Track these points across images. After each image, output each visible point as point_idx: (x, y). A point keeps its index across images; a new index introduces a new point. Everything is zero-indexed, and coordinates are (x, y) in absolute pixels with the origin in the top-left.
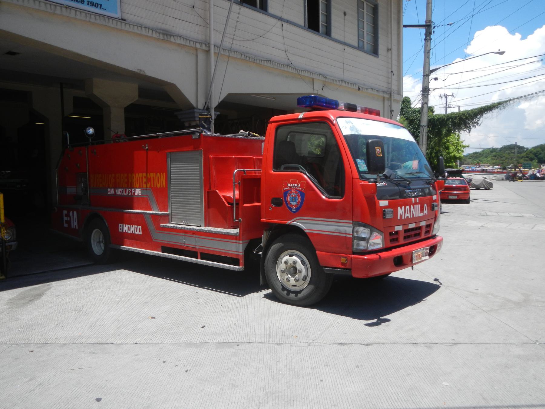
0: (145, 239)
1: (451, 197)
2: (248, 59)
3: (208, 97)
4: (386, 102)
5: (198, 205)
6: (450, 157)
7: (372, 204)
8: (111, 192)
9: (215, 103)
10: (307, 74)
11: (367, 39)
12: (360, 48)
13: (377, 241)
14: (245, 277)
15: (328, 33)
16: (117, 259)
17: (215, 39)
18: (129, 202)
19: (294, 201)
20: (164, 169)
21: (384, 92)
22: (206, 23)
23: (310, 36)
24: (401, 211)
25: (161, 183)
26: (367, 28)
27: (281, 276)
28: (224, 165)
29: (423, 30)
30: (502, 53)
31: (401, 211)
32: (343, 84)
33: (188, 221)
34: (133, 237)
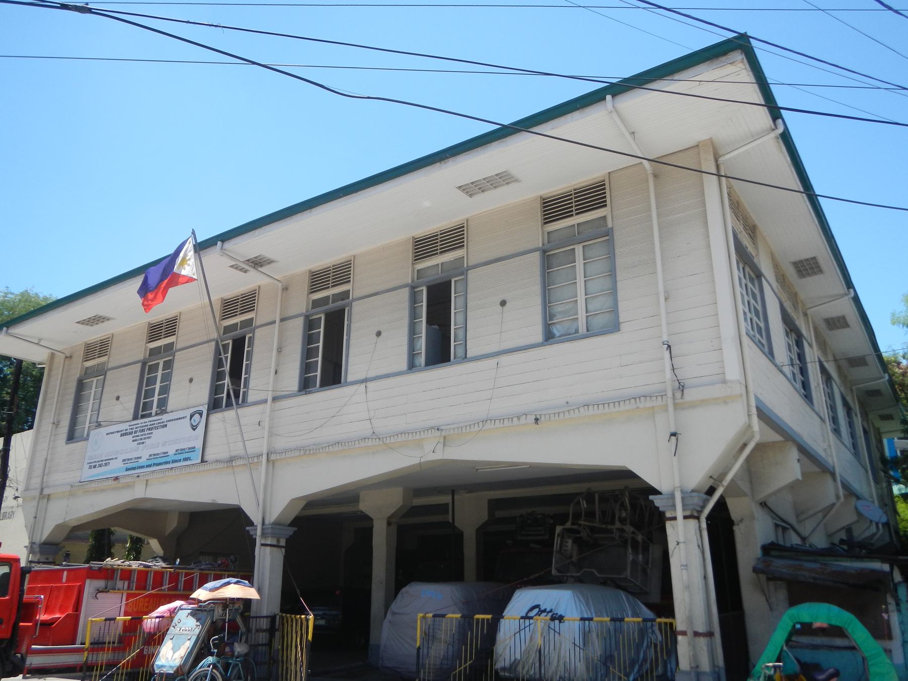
10: (400, 439)
32: (488, 426)
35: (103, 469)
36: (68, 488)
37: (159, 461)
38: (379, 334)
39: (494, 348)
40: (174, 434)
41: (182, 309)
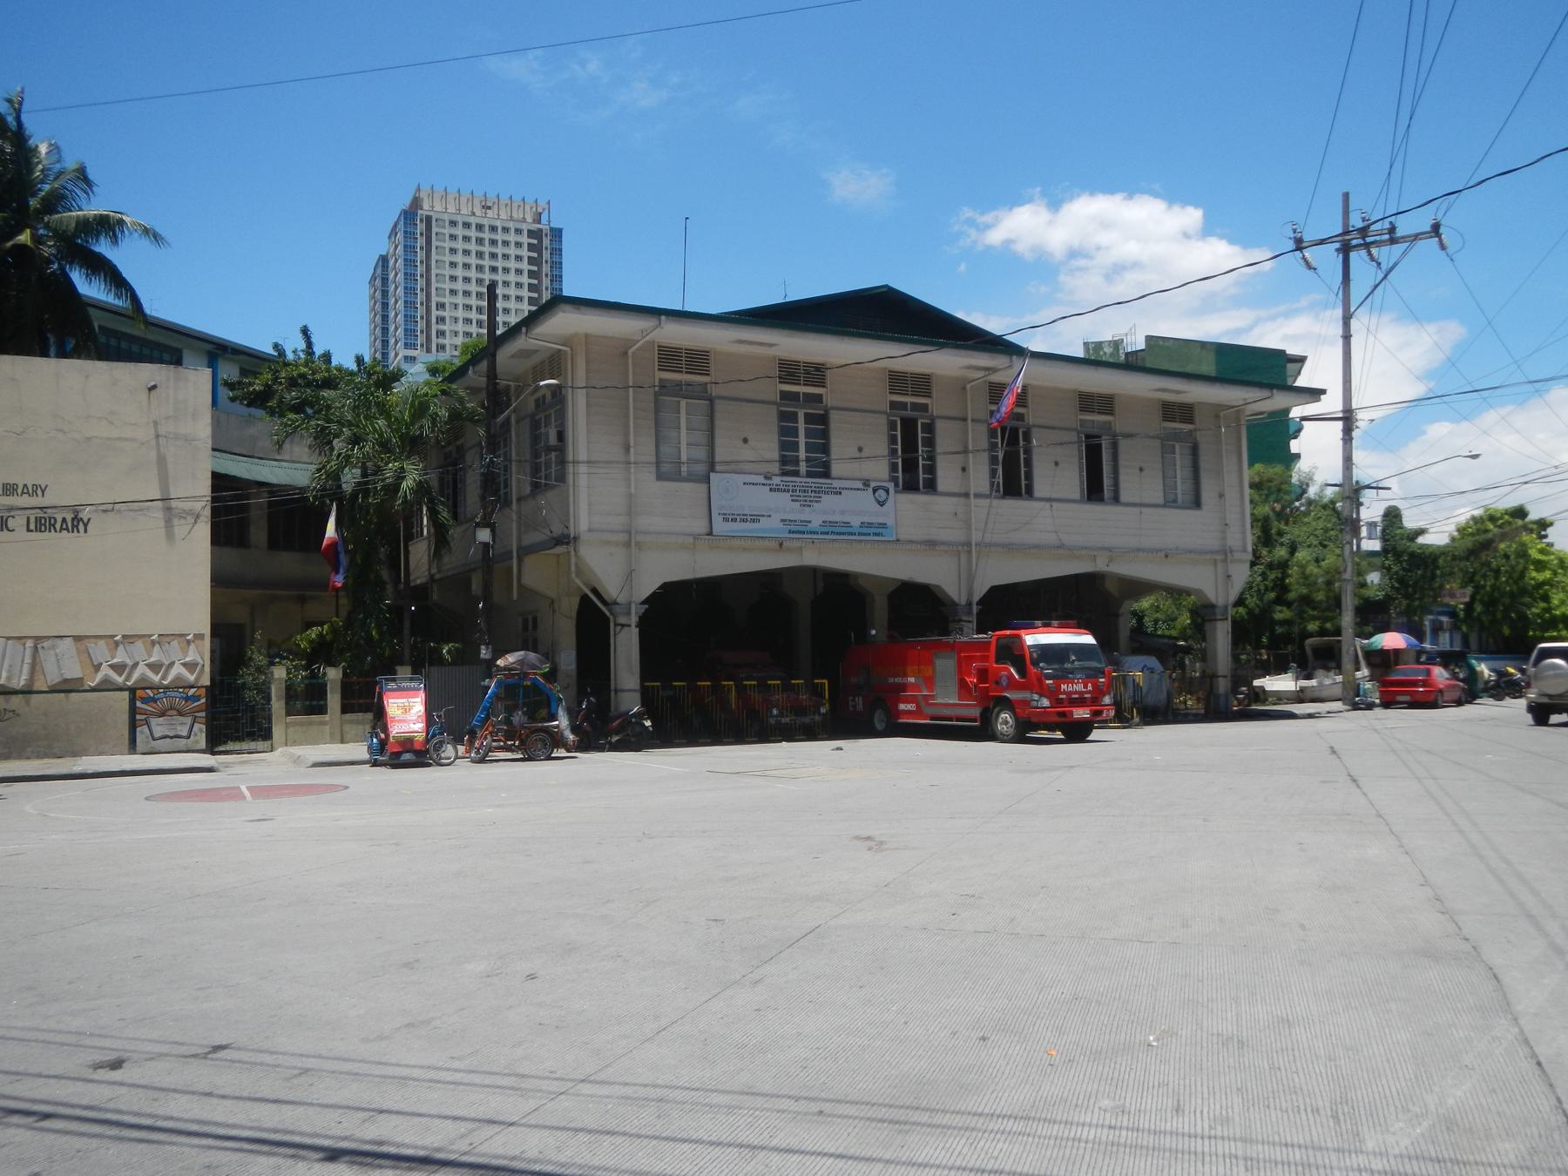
0: (918, 713)
1: (1400, 698)
2: (1010, 548)
3: (970, 593)
4: (1220, 565)
5: (953, 687)
6: (553, 705)
7: (1041, 682)
8: (891, 680)
9: (976, 598)
11: (1182, 488)
12: (1170, 502)
13: (1046, 702)
14: (982, 731)
15: (1116, 499)
16: (897, 729)
17: (976, 537)
18: (904, 687)
19: (1004, 682)
20: (930, 663)
21: (1212, 552)
22: (968, 524)
24: (1064, 687)
26: (1182, 473)
29: (1340, 424)
30: (1475, 457)
31: (1064, 687)
33: (947, 698)
34: (909, 712)
36: (691, 539)
37: (836, 531)
38: (1057, 464)
39: (1138, 501)
40: (850, 505)
41: (938, 372)
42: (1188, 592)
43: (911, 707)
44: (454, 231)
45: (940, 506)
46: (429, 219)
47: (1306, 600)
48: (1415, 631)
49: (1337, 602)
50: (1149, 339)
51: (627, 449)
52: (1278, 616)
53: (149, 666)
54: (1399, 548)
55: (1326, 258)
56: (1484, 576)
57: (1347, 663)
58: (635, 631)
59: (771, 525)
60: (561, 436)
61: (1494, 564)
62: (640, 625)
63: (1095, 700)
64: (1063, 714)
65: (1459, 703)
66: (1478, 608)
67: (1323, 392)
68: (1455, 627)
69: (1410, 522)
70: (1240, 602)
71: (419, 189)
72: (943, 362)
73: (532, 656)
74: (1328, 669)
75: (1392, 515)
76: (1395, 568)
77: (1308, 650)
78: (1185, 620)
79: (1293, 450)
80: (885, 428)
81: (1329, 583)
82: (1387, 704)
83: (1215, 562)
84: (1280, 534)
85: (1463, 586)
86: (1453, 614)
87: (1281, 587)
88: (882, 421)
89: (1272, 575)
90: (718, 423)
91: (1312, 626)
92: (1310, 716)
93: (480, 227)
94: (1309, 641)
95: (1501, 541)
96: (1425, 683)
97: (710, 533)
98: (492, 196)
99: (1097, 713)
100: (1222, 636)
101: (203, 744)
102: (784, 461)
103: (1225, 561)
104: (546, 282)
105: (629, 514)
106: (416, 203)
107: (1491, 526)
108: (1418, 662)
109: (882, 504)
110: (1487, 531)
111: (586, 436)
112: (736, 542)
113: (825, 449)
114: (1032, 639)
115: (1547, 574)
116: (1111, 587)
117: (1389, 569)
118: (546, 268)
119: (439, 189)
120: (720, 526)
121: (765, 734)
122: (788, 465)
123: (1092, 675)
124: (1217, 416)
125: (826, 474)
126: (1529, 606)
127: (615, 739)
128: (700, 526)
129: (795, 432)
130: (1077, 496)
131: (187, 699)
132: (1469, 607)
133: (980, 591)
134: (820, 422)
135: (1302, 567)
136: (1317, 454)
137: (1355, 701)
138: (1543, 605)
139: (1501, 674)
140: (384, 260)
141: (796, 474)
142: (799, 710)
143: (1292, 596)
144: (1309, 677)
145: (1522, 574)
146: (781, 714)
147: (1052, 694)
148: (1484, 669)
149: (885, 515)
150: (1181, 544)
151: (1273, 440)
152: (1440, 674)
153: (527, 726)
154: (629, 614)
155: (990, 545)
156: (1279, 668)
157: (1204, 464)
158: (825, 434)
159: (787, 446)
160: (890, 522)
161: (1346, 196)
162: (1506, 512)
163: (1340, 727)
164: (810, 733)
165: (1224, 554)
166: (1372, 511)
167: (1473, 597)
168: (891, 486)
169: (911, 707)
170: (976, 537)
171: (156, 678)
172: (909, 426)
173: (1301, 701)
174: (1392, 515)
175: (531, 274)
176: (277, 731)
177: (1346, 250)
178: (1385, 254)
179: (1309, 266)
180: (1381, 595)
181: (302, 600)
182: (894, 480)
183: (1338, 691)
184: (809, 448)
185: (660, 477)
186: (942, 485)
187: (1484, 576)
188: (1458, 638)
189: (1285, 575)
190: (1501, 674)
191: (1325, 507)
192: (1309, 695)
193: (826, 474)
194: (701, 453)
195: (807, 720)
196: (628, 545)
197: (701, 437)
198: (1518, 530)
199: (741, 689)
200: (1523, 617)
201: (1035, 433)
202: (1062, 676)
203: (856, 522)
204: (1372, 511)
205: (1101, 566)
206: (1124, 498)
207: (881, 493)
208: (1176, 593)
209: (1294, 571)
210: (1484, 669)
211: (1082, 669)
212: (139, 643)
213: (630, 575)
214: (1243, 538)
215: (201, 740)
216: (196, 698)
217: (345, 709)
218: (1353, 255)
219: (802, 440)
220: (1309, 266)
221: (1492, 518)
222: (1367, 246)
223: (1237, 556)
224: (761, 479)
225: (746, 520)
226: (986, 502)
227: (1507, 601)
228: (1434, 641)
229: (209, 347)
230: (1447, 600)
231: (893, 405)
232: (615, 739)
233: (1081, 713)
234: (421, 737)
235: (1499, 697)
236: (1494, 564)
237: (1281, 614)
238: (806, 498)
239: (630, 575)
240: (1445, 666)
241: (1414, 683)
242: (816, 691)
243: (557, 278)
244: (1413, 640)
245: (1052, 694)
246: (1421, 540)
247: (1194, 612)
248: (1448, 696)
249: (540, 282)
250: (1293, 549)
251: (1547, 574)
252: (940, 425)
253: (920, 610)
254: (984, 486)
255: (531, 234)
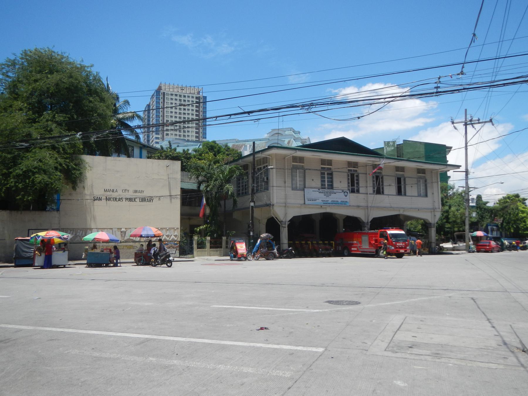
0: (358, 250)
2: (378, 208)
7: (392, 244)
11: (422, 192)
12: (419, 195)
13: (393, 248)
14: (375, 255)
15: (405, 195)
20: (361, 238)
22: (367, 202)
23: (399, 197)
25: (360, 240)
26: (422, 188)
27: (381, 254)
28: (372, 237)
30: (502, 183)
35: (314, 202)
37: (335, 203)
40: (338, 197)
42: (421, 219)
43: (355, 249)
44: (172, 97)
45: (360, 196)
46: (164, 93)
47: (455, 222)
48: (486, 230)
49: (464, 223)
50: (404, 141)
51: (285, 182)
52: (447, 226)
53: (167, 236)
54: (482, 207)
55: (461, 127)
56: (506, 215)
57: (467, 240)
58: (287, 228)
59: (319, 202)
60: (267, 179)
61: (509, 211)
62: (288, 227)
63: (405, 248)
64: (397, 251)
65: (498, 251)
66: (505, 224)
67: (461, 166)
68: (498, 230)
69: (484, 199)
70: (437, 223)
71: (161, 84)
72: (361, 159)
73: (269, 235)
74: (461, 241)
75: (479, 197)
76: (480, 213)
77: (455, 236)
78: (420, 227)
79: (448, 175)
80: (346, 176)
81: (461, 218)
82: (478, 251)
83: (431, 212)
84: (446, 202)
85: (500, 218)
86: (497, 226)
87: (447, 218)
88: (346, 174)
89: (445, 215)
90: (306, 176)
91: (456, 229)
92: (457, 254)
93: (180, 96)
94: (456, 233)
95: (511, 203)
96: (489, 246)
97: (305, 204)
98: (184, 86)
99: (406, 251)
100: (433, 232)
101: (178, 256)
102: (322, 185)
103: (434, 211)
104: (201, 113)
105: (286, 199)
106: (160, 88)
107: (508, 200)
108: (487, 240)
109: (346, 196)
110: (507, 202)
111: (275, 179)
112: (311, 206)
113: (332, 182)
114: (390, 232)
115: (525, 215)
116: (401, 218)
117: (478, 213)
118: (201, 109)
119: (167, 84)
120: (307, 202)
121: (318, 255)
122: (323, 186)
123: (404, 241)
124: (432, 172)
125: (332, 188)
126: (520, 224)
127: (285, 255)
128: (302, 202)
129: (324, 178)
130: (395, 194)
131: (175, 244)
132: (502, 224)
133: (370, 219)
134: (331, 175)
135: (454, 212)
136: (456, 179)
137: (469, 250)
138: (524, 224)
139: (511, 244)
140: (149, 106)
141: (325, 188)
142: (327, 249)
143: (450, 220)
144: (455, 244)
145: (518, 214)
146: (322, 250)
147: (395, 246)
148: (506, 242)
149: (347, 199)
150: (423, 207)
151: (445, 178)
152: (493, 243)
153: (269, 251)
154: (285, 224)
155: (374, 207)
156: (447, 241)
157: (428, 185)
158: (332, 178)
159: (323, 181)
160: (348, 201)
161: (466, 110)
162: (513, 196)
163: (465, 256)
164: (329, 255)
165: (434, 210)
166: (473, 195)
167: (503, 221)
168: (348, 191)
169: (355, 249)
170: (370, 205)
171: (168, 239)
172: (352, 176)
173: (454, 250)
174: (479, 197)
175: (197, 111)
176: (195, 252)
177: (466, 125)
178: (477, 126)
179: (455, 128)
180: (476, 220)
181: (189, 219)
182: (349, 190)
183: (464, 248)
184: (328, 182)
185: (293, 189)
186: (361, 191)
187: (506, 215)
188: (499, 233)
189: (449, 215)
190: (511, 244)
191: (459, 195)
192: (456, 249)
193: (332, 188)
194: (302, 183)
195: (328, 252)
196: (285, 207)
197: (302, 179)
198: (517, 201)
199: (312, 243)
200: (518, 227)
201: (385, 178)
202: (397, 241)
203: (340, 201)
204: (473, 195)
205: (401, 212)
206: (407, 194)
207: (346, 193)
208: (417, 219)
209: (451, 214)
210: (506, 242)
211: (402, 240)
212: (164, 230)
213: (286, 214)
214: (438, 204)
215: (178, 255)
216: (177, 244)
217: (211, 247)
218: (468, 126)
219: (326, 180)
220: (455, 128)
221: (509, 198)
222: (472, 124)
223: (438, 210)
224: (317, 190)
225: (313, 201)
226: (373, 195)
227: (513, 222)
228: (492, 234)
229: (140, 145)
230: (495, 222)
231: (349, 170)
232: (285, 255)
233: (402, 251)
234: (245, 253)
235: (510, 250)
236: (509, 211)
237: (448, 225)
238: (327, 195)
239: (286, 214)
240: (495, 241)
241: (486, 246)
242: (331, 245)
243: (205, 112)
244: (486, 234)
245: (395, 246)
246: (488, 205)
247: (422, 225)
248: (495, 249)
249: (199, 113)
250: (450, 207)
251: (525, 215)
252: (360, 175)
253: (353, 224)
254: (371, 192)
255: (197, 98)
